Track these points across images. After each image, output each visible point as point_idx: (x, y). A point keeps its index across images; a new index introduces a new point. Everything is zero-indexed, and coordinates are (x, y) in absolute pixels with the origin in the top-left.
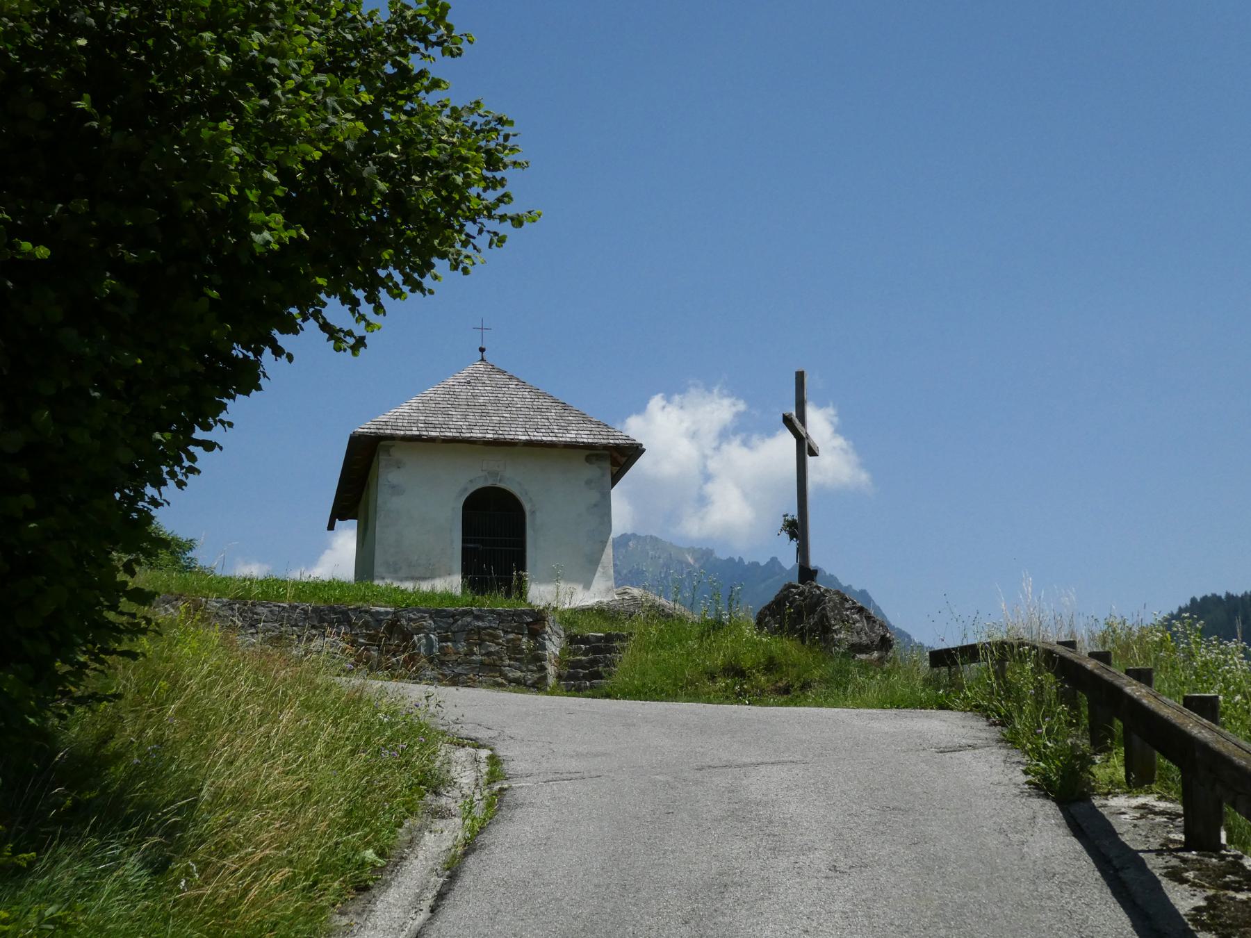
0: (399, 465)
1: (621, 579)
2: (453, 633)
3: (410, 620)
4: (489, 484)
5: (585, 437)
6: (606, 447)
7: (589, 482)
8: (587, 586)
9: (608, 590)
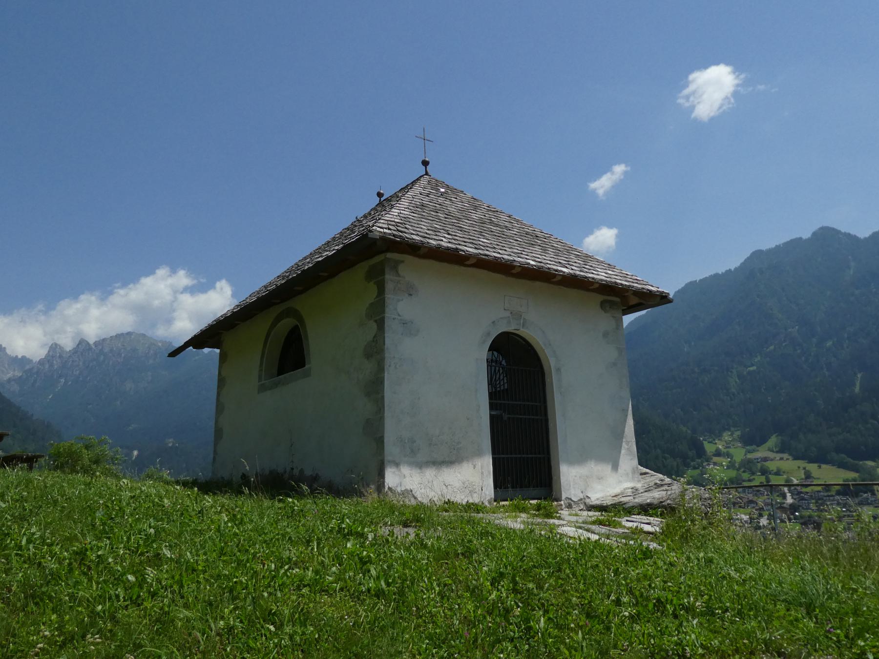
0: (410, 291)
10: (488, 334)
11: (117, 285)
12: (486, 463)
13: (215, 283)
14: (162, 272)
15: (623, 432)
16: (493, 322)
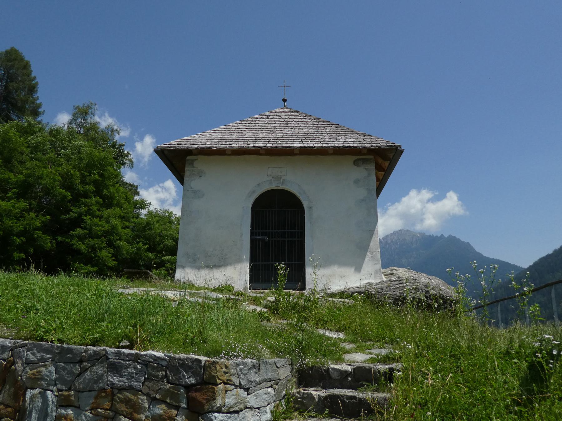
0: (200, 174)
1: (388, 261)
2: (78, 391)
3: (28, 363)
4: (273, 187)
5: (351, 142)
6: (371, 151)
7: (357, 182)
8: (358, 269)
9: (376, 272)
10: (254, 192)
11: (388, 204)
12: (245, 268)
13: (446, 194)
14: (413, 193)
15: (369, 246)
16: (259, 185)
